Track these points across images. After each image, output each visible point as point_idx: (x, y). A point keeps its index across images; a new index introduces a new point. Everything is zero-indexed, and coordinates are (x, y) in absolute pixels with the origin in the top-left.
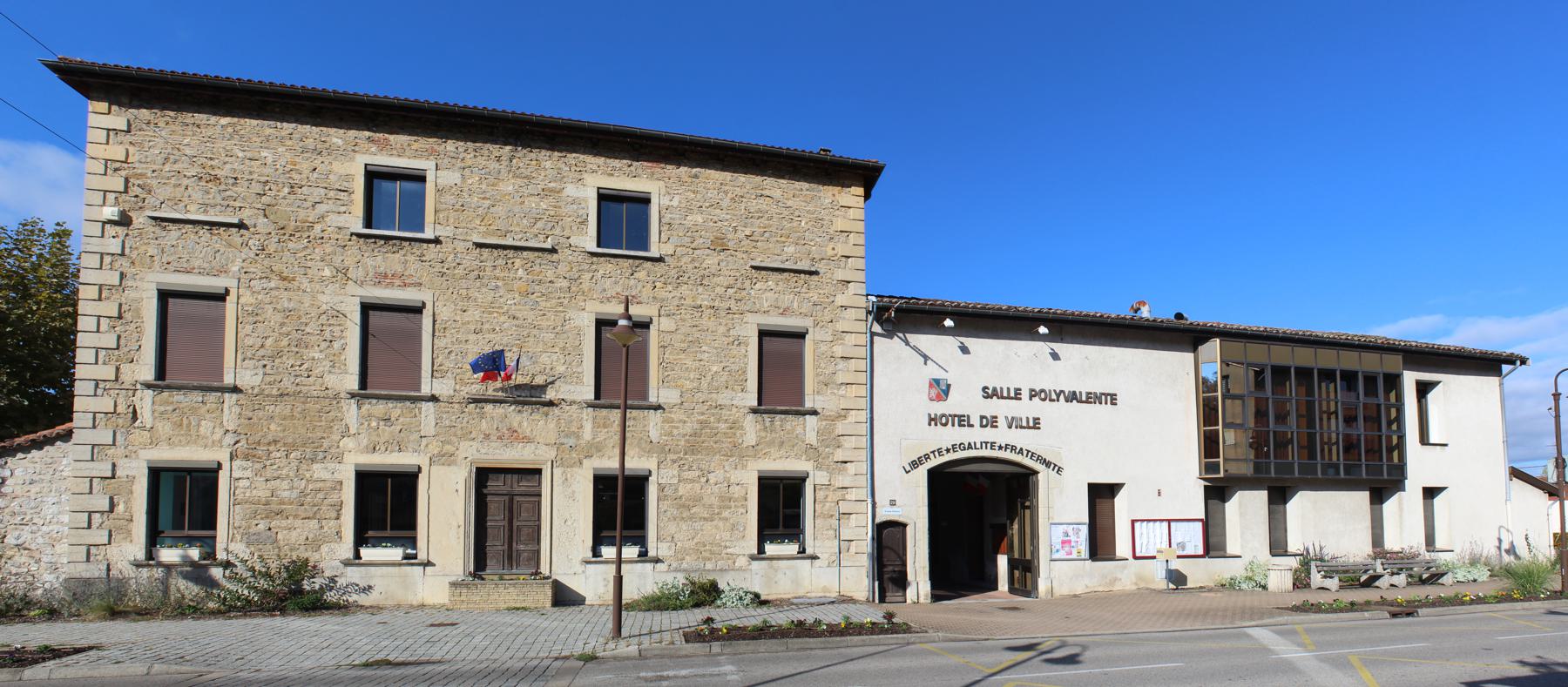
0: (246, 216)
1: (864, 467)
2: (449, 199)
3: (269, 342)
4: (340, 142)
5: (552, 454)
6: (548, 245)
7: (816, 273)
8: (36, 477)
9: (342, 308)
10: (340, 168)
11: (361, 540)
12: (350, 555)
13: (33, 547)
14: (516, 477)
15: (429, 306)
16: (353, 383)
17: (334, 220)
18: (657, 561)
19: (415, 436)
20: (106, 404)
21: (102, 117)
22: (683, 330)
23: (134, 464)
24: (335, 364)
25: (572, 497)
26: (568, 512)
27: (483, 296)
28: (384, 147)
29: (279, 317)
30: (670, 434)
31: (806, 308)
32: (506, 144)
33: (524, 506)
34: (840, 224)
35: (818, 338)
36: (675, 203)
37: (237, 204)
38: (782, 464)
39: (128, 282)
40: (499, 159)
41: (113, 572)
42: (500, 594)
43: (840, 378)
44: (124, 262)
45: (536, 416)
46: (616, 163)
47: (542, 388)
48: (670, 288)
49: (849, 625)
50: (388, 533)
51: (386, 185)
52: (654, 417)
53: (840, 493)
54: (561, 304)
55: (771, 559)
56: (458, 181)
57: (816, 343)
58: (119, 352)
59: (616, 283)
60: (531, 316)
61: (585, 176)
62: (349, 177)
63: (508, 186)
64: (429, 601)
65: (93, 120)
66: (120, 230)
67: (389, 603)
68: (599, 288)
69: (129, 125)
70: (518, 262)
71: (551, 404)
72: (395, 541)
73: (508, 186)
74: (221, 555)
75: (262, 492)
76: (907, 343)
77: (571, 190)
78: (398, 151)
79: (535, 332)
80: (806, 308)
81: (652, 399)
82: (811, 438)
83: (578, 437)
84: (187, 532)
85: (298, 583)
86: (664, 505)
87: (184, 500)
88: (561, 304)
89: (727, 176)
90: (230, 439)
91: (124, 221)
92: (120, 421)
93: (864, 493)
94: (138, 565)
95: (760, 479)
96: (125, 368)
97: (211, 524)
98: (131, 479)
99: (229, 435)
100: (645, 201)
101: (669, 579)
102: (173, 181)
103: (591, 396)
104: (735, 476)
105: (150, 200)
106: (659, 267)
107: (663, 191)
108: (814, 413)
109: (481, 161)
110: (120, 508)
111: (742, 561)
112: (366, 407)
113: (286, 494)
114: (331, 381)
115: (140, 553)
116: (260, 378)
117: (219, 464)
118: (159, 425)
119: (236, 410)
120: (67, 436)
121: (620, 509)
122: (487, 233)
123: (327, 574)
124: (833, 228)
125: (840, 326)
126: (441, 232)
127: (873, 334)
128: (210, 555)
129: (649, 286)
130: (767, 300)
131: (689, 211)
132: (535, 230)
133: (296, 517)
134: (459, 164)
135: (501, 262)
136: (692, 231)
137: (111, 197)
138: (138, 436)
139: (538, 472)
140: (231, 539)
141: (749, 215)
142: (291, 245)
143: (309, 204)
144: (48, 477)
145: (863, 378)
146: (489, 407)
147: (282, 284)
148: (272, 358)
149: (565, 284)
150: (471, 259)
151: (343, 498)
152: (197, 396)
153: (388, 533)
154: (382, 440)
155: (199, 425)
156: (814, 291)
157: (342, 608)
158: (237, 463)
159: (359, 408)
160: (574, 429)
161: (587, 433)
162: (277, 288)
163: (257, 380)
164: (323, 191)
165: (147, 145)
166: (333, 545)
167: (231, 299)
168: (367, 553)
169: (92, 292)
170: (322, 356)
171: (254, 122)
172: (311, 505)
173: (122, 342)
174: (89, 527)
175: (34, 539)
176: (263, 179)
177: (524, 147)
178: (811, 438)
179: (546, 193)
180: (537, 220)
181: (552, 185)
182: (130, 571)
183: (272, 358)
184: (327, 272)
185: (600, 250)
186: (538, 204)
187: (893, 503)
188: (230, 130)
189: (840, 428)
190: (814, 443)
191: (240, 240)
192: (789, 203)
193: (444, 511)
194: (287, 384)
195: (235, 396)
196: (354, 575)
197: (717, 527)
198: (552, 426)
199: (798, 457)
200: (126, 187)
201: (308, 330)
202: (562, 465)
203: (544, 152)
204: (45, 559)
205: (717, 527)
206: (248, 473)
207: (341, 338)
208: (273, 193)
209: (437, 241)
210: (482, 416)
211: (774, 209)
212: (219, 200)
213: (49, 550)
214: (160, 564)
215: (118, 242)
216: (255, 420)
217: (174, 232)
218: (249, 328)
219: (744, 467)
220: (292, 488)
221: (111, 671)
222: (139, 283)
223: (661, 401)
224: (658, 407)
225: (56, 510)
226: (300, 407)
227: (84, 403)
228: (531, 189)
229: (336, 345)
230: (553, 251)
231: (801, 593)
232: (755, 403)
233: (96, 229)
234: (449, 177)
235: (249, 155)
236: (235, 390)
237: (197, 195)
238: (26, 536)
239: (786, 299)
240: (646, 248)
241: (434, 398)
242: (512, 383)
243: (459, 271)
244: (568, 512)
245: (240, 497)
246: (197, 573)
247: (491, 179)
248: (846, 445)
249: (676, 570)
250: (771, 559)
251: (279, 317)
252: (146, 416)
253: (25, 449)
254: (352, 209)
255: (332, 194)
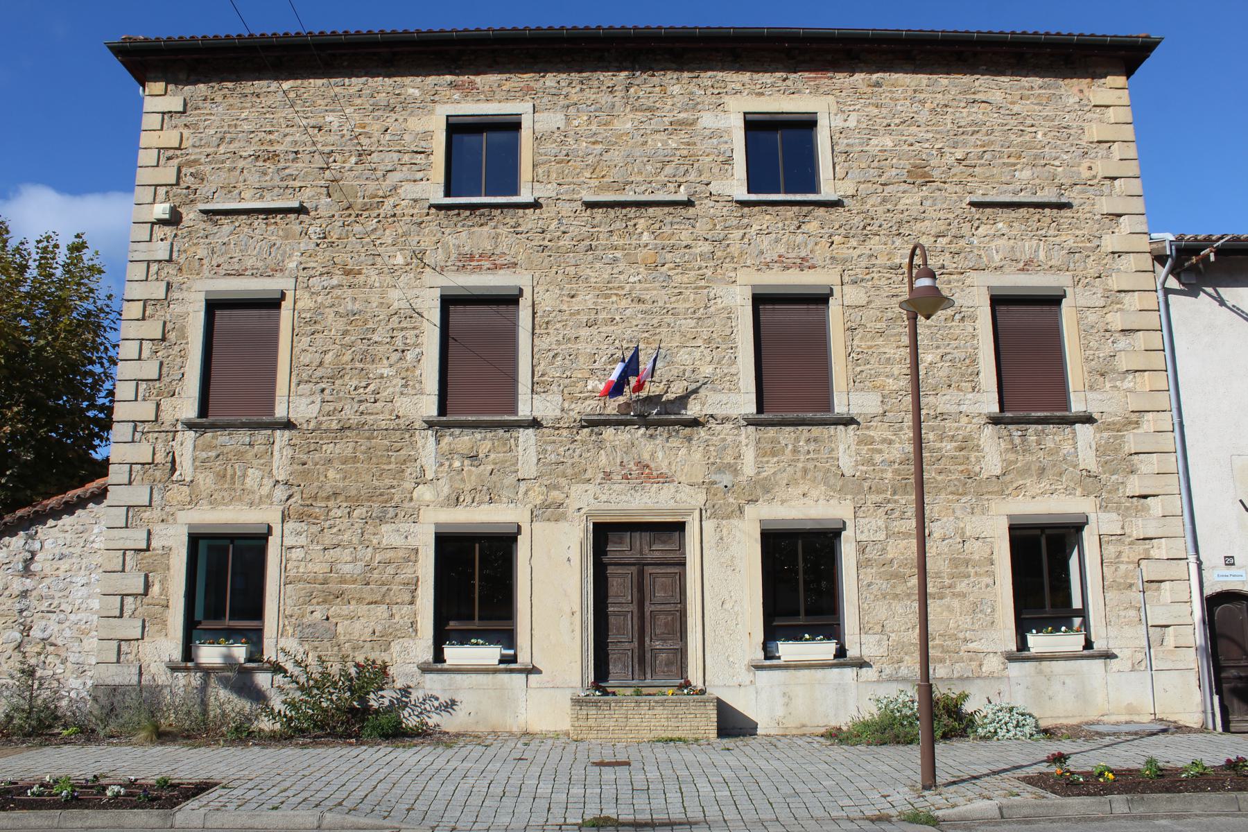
0: (306, 197)
1: (1177, 504)
2: (551, 148)
3: (329, 358)
4: (417, 92)
5: (699, 498)
6: (682, 195)
7: (1068, 206)
8: (66, 551)
9: (418, 304)
10: (416, 124)
11: (441, 637)
12: (429, 656)
13: (59, 642)
14: (646, 536)
15: (527, 293)
16: (430, 407)
17: (409, 191)
18: (861, 664)
19: (511, 479)
20: (142, 452)
21: (159, 99)
22: (877, 303)
23: (171, 530)
24: (409, 382)
25: (731, 566)
26: (725, 588)
27: (597, 273)
28: (469, 92)
29: (341, 324)
30: (870, 462)
31: (1058, 258)
32: (620, 70)
33: (659, 581)
34: (1095, 131)
35: (1082, 302)
36: (852, 123)
37: (297, 184)
38: (802, 507)
39: (175, 295)
40: (611, 90)
41: (146, 679)
42: (639, 719)
43: (1123, 363)
44: (171, 269)
45: (674, 442)
46: (767, 78)
47: (683, 400)
48: (853, 242)
49: (1161, 773)
50: (476, 624)
51: (469, 139)
52: (844, 436)
53: (1140, 548)
54: (702, 277)
55: (1039, 658)
56: (562, 125)
57: (1081, 310)
58: (160, 386)
59: (777, 241)
60: (662, 296)
61: (726, 99)
62: (427, 135)
63: (625, 124)
64: (535, 727)
65: (150, 104)
66: (168, 231)
67: (481, 729)
68: (753, 250)
69: (185, 104)
70: (642, 223)
71: (695, 423)
72: (490, 637)
73: (625, 124)
74: (270, 653)
75: (319, 568)
76: (1222, 303)
77: (708, 120)
78: (489, 96)
79: (669, 319)
80: (1058, 258)
81: (840, 408)
82: (1088, 460)
83: (736, 472)
84: (228, 623)
85: (363, 700)
86: (869, 574)
87: (226, 579)
88: (702, 277)
89: (923, 79)
90: (280, 493)
91: (174, 219)
92: (158, 474)
93: (1181, 546)
94: (174, 668)
95: (1012, 528)
96: (166, 404)
97: (257, 612)
98: (167, 551)
99: (280, 487)
100: (512, 126)
101: (890, 691)
102: (228, 165)
103: (751, 408)
104: (972, 525)
105: (205, 190)
106: (838, 215)
107: (834, 108)
108: (1088, 419)
109: (589, 95)
110: (155, 590)
111: (993, 664)
112: (447, 440)
113: (347, 568)
114: (404, 406)
115: (174, 650)
116: (316, 407)
117: (270, 528)
118: (200, 477)
119: (288, 452)
120: (100, 496)
121: (801, 584)
122: (601, 188)
123: (399, 685)
124: (1086, 138)
125: (1114, 283)
126: (543, 192)
127: (1167, 292)
128: (255, 655)
129: (824, 242)
130: (998, 250)
131: (873, 132)
132: (662, 178)
133: (360, 600)
134: (563, 102)
135: (619, 225)
136: (880, 161)
137: (162, 191)
138: (178, 494)
139: (680, 527)
140: (281, 633)
141: (960, 131)
142: (357, 228)
143: (379, 174)
144: (78, 550)
145: (1158, 360)
146: (609, 432)
147: (345, 280)
148: (332, 379)
149: (706, 247)
150: (580, 224)
151: (419, 574)
152: (243, 436)
153: (476, 624)
154: (468, 487)
155: (244, 476)
156: (1067, 233)
157: (422, 734)
158: (290, 525)
159: (438, 442)
160: (729, 459)
161: (749, 466)
162: (340, 286)
163: (313, 411)
164: (395, 156)
165: (202, 125)
166: (406, 642)
167: (286, 305)
168: (455, 654)
169: (134, 310)
170: (392, 372)
171: (319, 82)
172: (379, 587)
173: (165, 370)
174: (121, 616)
175: (61, 631)
176: (327, 149)
177: (644, 71)
178: (1088, 460)
179: (678, 126)
180: (665, 164)
181: (682, 115)
182: (163, 678)
183: (332, 379)
184: (400, 260)
185: (753, 197)
186: (665, 143)
187: (1229, 561)
188: (292, 95)
189: (1132, 441)
190: (1093, 467)
191: (298, 228)
192: (1016, 108)
193: (553, 588)
194: (349, 413)
195: (287, 433)
196: (434, 684)
197: (950, 609)
198: (698, 456)
199: (1069, 491)
200: (178, 178)
201: (376, 338)
202: (714, 515)
203: (669, 74)
204: (72, 658)
205: (950, 609)
206: (302, 540)
207: (416, 345)
208: (338, 165)
209: (536, 205)
210: (600, 445)
211: (994, 119)
212: (277, 182)
213: (75, 646)
214: (198, 668)
215: (167, 244)
216: (310, 465)
217: (227, 225)
218: (306, 340)
219: (985, 511)
220: (355, 560)
221: (228, 819)
222: (185, 294)
223: (854, 411)
224: (849, 421)
225: (82, 595)
226: (364, 444)
227: (119, 450)
228: (655, 124)
229: (410, 356)
230: (689, 204)
231: (1092, 715)
232: (995, 408)
233: (144, 233)
234: (551, 120)
235: (312, 122)
236: (288, 425)
237: (254, 179)
238: (53, 628)
239: (1027, 248)
240: (813, 187)
241: (535, 424)
242: (643, 394)
243: (565, 242)
244: (725, 588)
245: (292, 573)
246: (240, 680)
247: (603, 117)
248: (1143, 468)
249: (891, 679)
250: (1039, 658)
251: (341, 324)
252: (186, 468)
253: (56, 514)
254: (431, 174)
255: (406, 158)
